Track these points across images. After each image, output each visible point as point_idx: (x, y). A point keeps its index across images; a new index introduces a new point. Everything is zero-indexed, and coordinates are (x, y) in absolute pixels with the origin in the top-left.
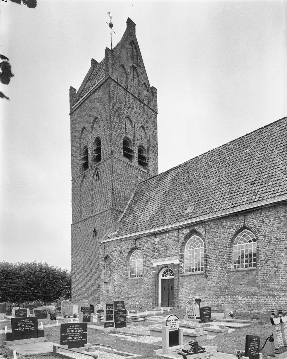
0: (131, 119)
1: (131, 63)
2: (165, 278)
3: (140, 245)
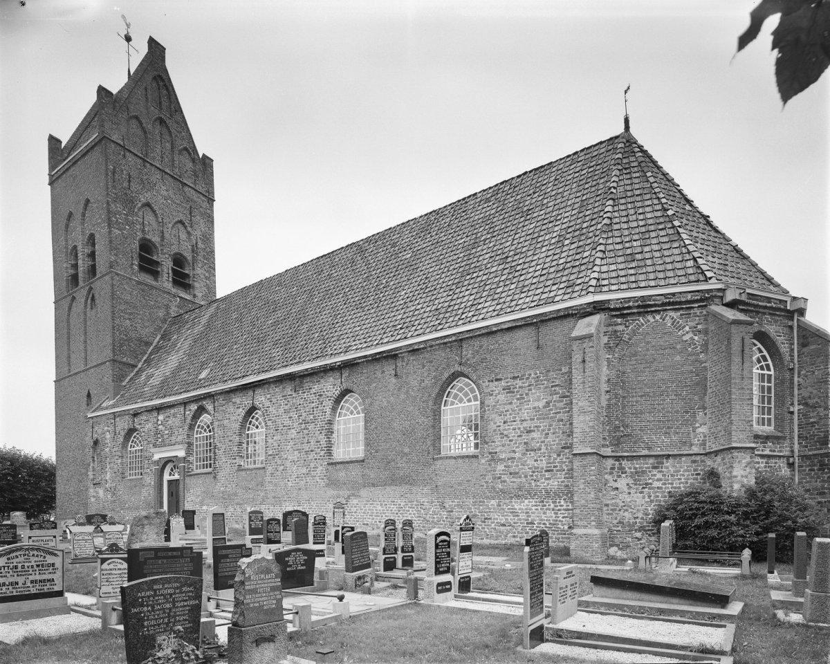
1: (155, 112)
2: (172, 478)
3: (140, 424)
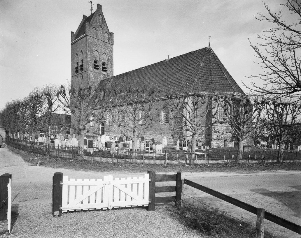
0: (98, 51)
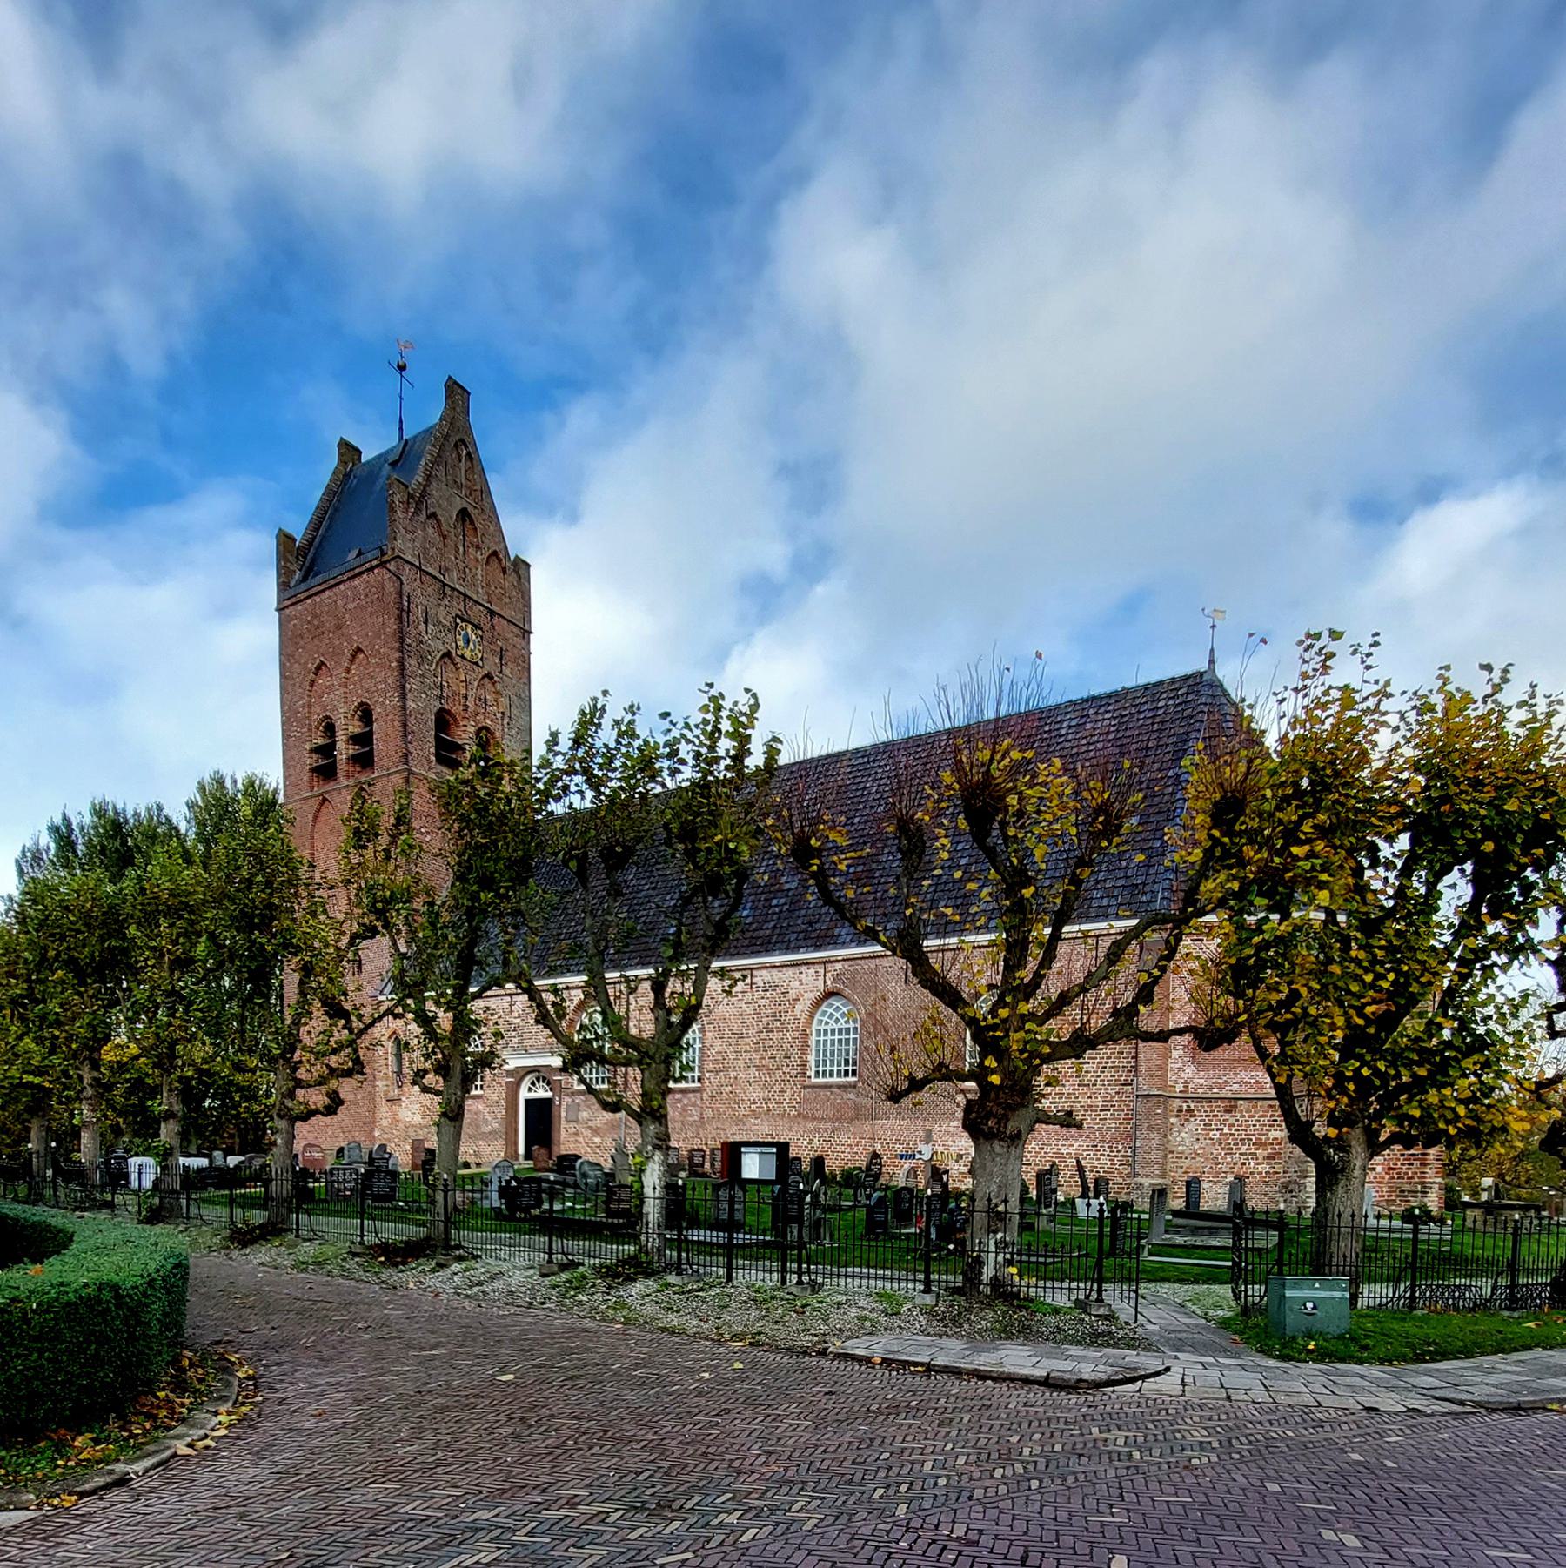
2: (533, 1095)
